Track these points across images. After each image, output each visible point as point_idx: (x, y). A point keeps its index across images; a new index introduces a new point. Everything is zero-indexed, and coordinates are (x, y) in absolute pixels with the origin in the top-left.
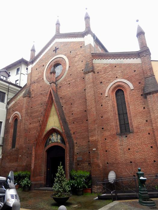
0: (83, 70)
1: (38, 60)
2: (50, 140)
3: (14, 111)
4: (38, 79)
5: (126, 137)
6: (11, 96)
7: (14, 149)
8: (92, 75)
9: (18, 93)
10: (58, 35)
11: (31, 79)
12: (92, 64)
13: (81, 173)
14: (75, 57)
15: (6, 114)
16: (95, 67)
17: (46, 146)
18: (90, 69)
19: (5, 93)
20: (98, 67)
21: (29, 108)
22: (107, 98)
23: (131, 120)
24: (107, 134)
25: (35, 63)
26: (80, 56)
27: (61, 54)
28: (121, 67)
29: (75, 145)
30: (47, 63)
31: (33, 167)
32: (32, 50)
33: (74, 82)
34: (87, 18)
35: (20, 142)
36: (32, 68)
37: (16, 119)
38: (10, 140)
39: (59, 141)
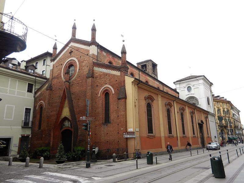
0: (87, 74)
1: (58, 59)
2: (64, 125)
3: (40, 100)
4: (58, 75)
5: (107, 125)
6: (38, 87)
7: (40, 130)
8: (91, 80)
9: (44, 83)
10: (74, 40)
11: (52, 75)
12: (93, 70)
13: (79, 148)
14: (83, 62)
15: (34, 102)
16: (95, 73)
17: (61, 129)
18: (92, 75)
19: (32, 85)
20: (96, 73)
21: (51, 99)
22: (99, 98)
23: (111, 114)
24: (97, 123)
25: (56, 61)
26: (86, 61)
27: (74, 57)
28: (109, 76)
29: (79, 129)
30: (65, 62)
31: (51, 144)
32: (73, 28)
33: (81, 82)
34: (94, 30)
35: (44, 126)
36: (53, 65)
37: (41, 107)
38: (37, 123)
39: (69, 126)
